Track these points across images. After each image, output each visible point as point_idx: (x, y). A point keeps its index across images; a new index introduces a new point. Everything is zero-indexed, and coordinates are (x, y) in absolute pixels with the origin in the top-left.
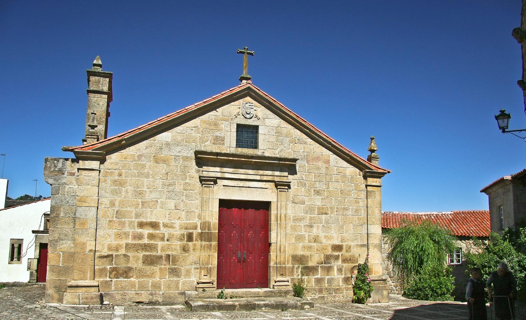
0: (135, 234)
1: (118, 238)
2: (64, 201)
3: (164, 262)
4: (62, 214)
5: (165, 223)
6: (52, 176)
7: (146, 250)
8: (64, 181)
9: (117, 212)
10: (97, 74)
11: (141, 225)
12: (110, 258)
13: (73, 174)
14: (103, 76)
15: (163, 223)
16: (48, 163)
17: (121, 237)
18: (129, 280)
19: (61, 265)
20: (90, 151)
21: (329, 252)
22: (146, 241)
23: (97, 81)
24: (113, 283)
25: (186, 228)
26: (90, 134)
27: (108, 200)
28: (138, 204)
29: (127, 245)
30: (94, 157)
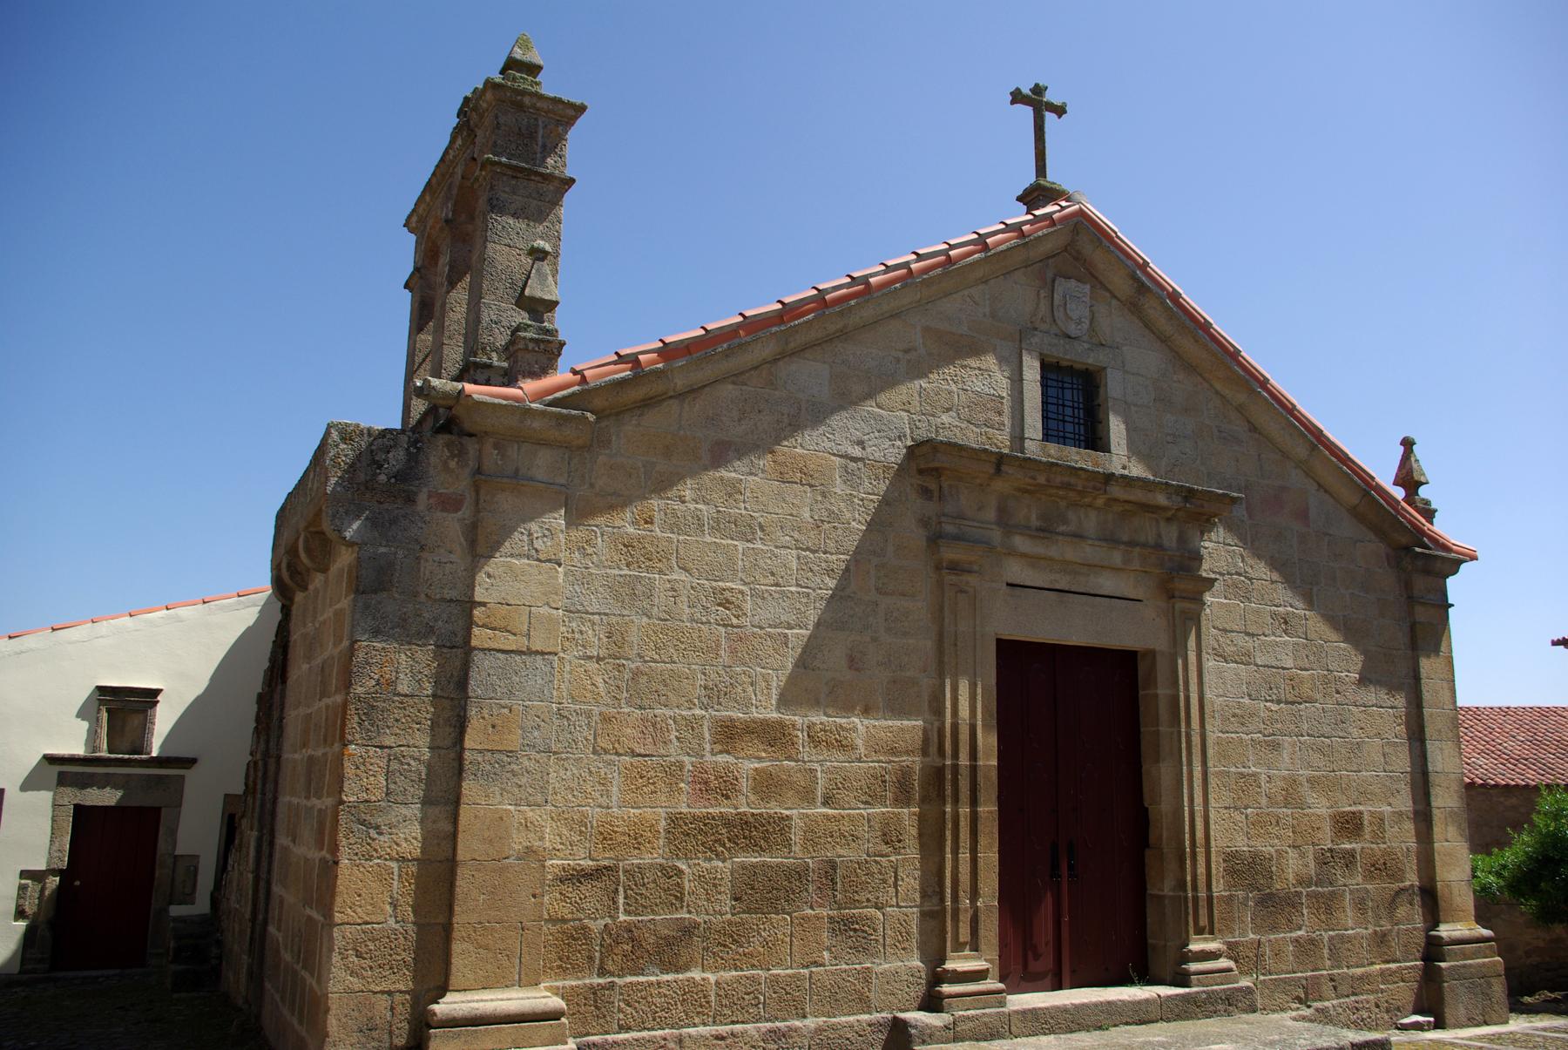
7: (754, 846)
11: (729, 734)
21: (1326, 839)
22: (746, 804)
25: (893, 751)
29: (674, 820)
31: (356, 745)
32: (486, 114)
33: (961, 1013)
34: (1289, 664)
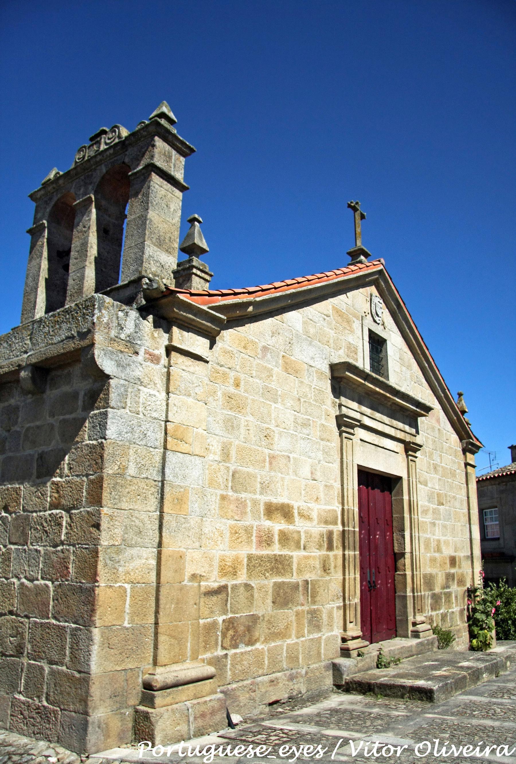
0: (261, 533)
1: (235, 541)
2: (137, 430)
3: (301, 598)
4: (132, 470)
5: (301, 508)
6: (112, 353)
8: (138, 373)
9: (233, 475)
10: (170, 137)
12: (223, 596)
13: (154, 359)
14: (178, 147)
15: (298, 508)
16: (104, 311)
17: (240, 540)
18: (253, 648)
19: (126, 624)
20: (205, 308)
23: (166, 153)
24: (229, 662)
26: (201, 268)
27: (218, 442)
28: (264, 461)
29: (250, 558)
30: (203, 327)
31: (108, 507)
32: (142, 139)
33: (127, 606)
34: (437, 488)
